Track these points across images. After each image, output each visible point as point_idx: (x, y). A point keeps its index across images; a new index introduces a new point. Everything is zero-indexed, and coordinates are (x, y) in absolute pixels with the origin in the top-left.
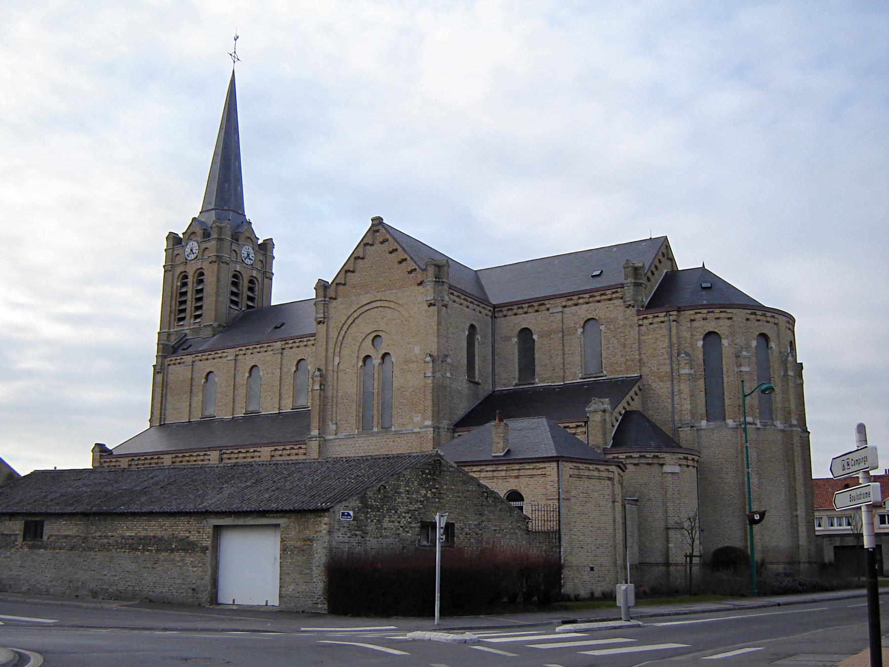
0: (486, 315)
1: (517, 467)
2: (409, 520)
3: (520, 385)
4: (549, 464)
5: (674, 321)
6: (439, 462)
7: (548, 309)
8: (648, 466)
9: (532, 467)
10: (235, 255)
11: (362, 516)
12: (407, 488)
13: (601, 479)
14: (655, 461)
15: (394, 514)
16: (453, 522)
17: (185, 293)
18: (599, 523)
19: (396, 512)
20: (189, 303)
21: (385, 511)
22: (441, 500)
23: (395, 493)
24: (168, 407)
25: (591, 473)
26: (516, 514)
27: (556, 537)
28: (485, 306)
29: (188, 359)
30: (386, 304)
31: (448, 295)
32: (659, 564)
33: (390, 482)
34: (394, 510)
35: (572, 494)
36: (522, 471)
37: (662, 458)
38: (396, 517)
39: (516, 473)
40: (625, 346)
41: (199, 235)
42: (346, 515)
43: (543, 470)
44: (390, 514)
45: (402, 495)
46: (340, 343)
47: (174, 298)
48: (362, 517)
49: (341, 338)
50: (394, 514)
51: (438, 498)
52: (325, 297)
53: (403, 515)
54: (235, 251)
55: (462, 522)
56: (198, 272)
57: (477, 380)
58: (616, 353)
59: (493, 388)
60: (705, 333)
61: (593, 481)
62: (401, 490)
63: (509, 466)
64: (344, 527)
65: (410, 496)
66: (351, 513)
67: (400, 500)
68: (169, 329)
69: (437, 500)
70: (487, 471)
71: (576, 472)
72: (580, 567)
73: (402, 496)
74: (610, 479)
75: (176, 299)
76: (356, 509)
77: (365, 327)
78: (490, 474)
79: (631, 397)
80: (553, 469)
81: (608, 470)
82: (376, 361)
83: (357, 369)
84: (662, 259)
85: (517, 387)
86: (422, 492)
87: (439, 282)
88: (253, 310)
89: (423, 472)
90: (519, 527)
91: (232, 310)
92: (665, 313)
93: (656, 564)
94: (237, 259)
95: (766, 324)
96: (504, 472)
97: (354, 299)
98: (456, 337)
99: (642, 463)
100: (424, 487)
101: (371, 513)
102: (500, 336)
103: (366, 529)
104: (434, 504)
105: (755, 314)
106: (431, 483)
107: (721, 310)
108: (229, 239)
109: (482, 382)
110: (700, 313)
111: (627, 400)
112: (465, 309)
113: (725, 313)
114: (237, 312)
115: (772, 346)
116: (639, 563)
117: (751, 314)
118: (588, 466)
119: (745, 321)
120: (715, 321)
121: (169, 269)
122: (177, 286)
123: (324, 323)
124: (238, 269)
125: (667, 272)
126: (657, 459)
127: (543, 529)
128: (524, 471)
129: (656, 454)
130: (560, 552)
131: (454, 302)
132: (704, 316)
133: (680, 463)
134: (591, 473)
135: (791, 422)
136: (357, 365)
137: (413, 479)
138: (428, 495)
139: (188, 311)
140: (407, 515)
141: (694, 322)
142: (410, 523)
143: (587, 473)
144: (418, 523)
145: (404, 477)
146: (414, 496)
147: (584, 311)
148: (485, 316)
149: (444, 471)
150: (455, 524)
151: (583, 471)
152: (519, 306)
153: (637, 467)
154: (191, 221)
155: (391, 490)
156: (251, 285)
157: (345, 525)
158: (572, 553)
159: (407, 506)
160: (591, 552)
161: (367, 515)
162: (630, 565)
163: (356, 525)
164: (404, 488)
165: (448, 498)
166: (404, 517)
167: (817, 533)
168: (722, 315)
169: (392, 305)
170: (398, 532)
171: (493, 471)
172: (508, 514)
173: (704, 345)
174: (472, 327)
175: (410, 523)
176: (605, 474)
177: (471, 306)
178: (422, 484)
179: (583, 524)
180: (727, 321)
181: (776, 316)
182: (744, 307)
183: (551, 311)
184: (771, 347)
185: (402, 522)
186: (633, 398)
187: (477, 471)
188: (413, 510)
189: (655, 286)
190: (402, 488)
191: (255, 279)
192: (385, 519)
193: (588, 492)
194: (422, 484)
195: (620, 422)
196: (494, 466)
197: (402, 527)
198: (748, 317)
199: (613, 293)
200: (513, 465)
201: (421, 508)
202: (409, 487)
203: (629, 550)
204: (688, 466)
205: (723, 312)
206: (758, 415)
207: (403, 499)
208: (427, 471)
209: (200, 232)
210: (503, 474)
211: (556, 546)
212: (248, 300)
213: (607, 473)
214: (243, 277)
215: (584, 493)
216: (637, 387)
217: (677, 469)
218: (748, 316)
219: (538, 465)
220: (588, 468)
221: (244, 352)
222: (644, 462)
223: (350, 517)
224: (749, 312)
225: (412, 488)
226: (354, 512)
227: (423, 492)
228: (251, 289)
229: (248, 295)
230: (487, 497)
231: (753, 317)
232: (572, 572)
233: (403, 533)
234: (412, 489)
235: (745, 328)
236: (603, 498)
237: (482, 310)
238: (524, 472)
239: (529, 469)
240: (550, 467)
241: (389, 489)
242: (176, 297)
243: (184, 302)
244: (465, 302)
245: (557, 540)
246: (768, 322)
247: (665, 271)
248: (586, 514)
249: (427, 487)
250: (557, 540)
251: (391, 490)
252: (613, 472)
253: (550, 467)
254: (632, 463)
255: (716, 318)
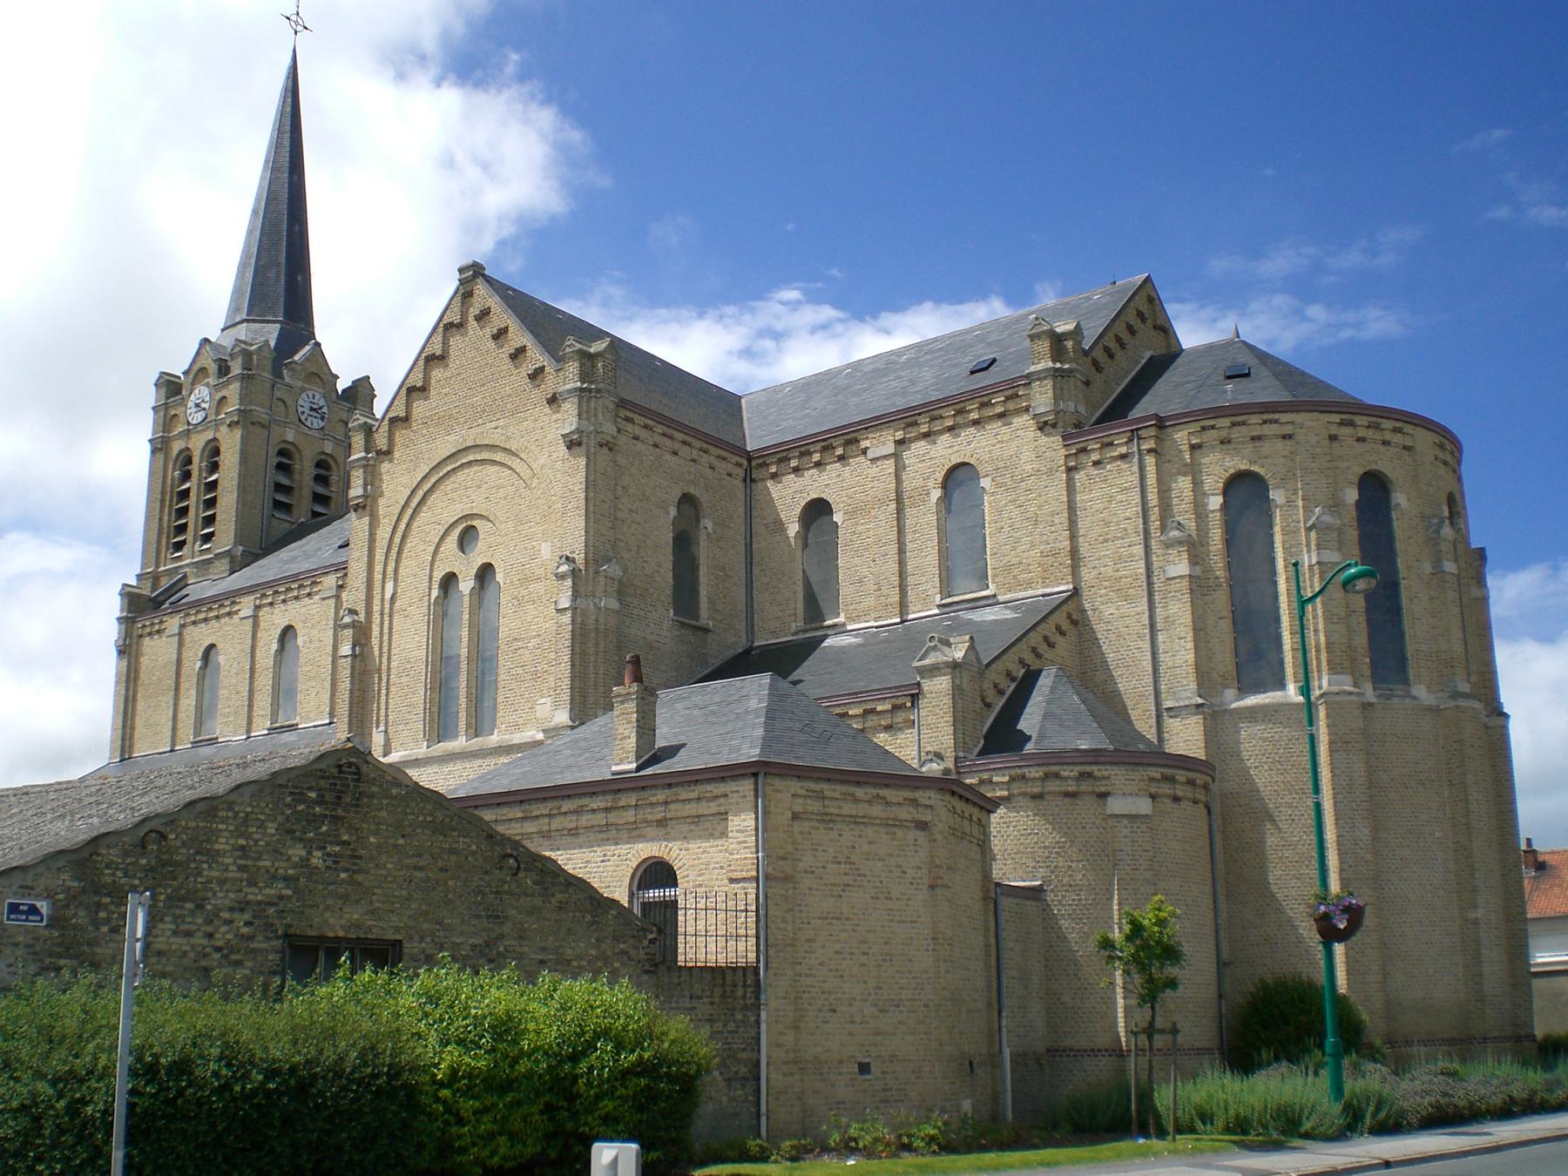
0: (729, 475)
1: (661, 796)
2: (245, 930)
3: (806, 631)
4: (733, 783)
5: (1149, 451)
6: (353, 769)
7: (864, 452)
8: (1067, 800)
9: (694, 795)
10: (282, 408)
11: (81, 917)
12: (242, 842)
13: (895, 825)
14: (1085, 786)
15: (192, 913)
16: (398, 937)
17: (185, 494)
18: (886, 943)
19: (200, 907)
20: (192, 512)
21: (161, 904)
22: (360, 878)
23: (197, 853)
24: (139, 722)
25: (861, 810)
26: (615, 917)
27: (745, 981)
28: (725, 454)
29: (173, 623)
30: (485, 455)
31: (615, 422)
32: (1099, 1050)
33: (184, 823)
34: (193, 901)
35: (800, 864)
36: (672, 806)
37: (1105, 778)
38: (200, 921)
39: (658, 813)
40: (1036, 523)
41: (210, 372)
42: (22, 912)
43: (722, 800)
44: (178, 912)
45: (220, 860)
46: (397, 550)
47: (167, 504)
48: (81, 917)
49: (397, 540)
50: (192, 913)
51: (346, 870)
52: (367, 451)
53: (226, 915)
54: (283, 402)
55: (429, 939)
56: (209, 447)
57: (703, 622)
58: (1018, 540)
59: (748, 641)
60: (1227, 475)
61: (870, 831)
62: (217, 847)
63: (643, 794)
64: (16, 945)
65: (250, 863)
66: (43, 906)
67: (216, 874)
68: (157, 566)
69: (343, 875)
70: (594, 811)
71: (814, 806)
72: (826, 1062)
73: (223, 864)
74: (922, 826)
75: (170, 506)
76: (61, 896)
77: (445, 509)
78: (600, 819)
79: (1046, 639)
80: (744, 796)
81: (915, 803)
82: (466, 585)
83: (429, 606)
84: (1137, 324)
85: (801, 636)
86: (290, 852)
87: (590, 391)
88: (320, 519)
89: (299, 797)
90: (624, 952)
91: (275, 522)
92: (1129, 434)
93: (1092, 1050)
94: (286, 417)
95: (1383, 449)
96: (632, 812)
97: (423, 447)
98: (640, 520)
99: (1050, 793)
100: (301, 840)
101: (112, 908)
102: (765, 522)
103: (94, 954)
104: (330, 888)
105: (1351, 424)
106: (324, 828)
107: (1265, 417)
108: (267, 375)
109: (714, 626)
110: (1213, 427)
111: (1033, 644)
112: (668, 457)
113: (1276, 425)
114: (287, 525)
115: (1399, 501)
116: (1048, 1050)
117: (1342, 424)
118: (852, 789)
119: (1327, 442)
120: (1251, 445)
121: (159, 446)
122: (173, 479)
123: (364, 507)
124: (328, 451)
125: (1151, 358)
126: (1091, 781)
127: (702, 957)
128: (679, 806)
129: (1088, 769)
130: (758, 1022)
131: (636, 438)
132: (1224, 433)
133: (1153, 790)
134: (861, 810)
135: (1456, 686)
136: (429, 595)
137: (262, 817)
138: (314, 861)
139: (191, 527)
140: (237, 915)
141: (1199, 451)
142: (251, 938)
143: (848, 809)
144: (277, 938)
145: (230, 809)
146: (261, 863)
147: (945, 451)
148: (726, 477)
149: (372, 796)
150: (406, 945)
151: (835, 803)
152: (803, 449)
153: (1038, 802)
154: (197, 346)
155: (184, 844)
156: (322, 472)
157: (20, 939)
158: (802, 1025)
159: (241, 890)
160: (861, 1023)
161: (97, 913)
162: (1011, 1055)
163: (59, 940)
164: (232, 841)
165: (383, 872)
166: (229, 922)
167: (1532, 970)
168: (1269, 430)
169: (498, 457)
170: (204, 963)
171: (607, 810)
172: (588, 918)
173: (1225, 506)
174: (687, 500)
175: (251, 938)
176: (904, 813)
177: (684, 451)
178: (293, 832)
179: (838, 947)
180: (1280, 444)
181: (1408, 428)
182: (1323, 409)
183: (870, 454)
184: (1398, 504)
185: (217, 936)
186: (1052, 640)
187: (571, 812)
188: (260, 903)
189: (1118, 385)
190: (223, 840)
191: (330, 461)
192: (161, 926)
193: (854, 858)
194: (293, 832)
195: (1010, 698)
196: (609, 797)
197: (218, 949)
198: (1333, 433)
199: (1008, 398)
200: (649, 792)
201: (289, 898)
202: (248, 837)
203: (1007, 1017)
204: (1176, 799)
205: (1271, 422)
206: (1367, 672)
207: (227, 870)
208: (313, 795)
209: (213, 368)
210: (629, 815)
211: (745, 1008)
212: (275, 490)
213: (911, 809)
214: (301, 455)
215: (840, 863)
216: (1065, 615)
217: (1144, 806)
218: (1334, 430)
219: (709, 788)
220: (853, 795)
221: (270, 600)
222: (1057, 789)
223: (39, 918)
224: (1336, 418)
225: (257, 841)
226: (54, 904)
227: (298, 852)
228: (322, 480)
229: (314, 493)
230: (519, 868)
231: (1346, 431)
232: (797, 1077)
233: (220, 966)
234: (256, 845)
235: (1328, 458)
236: (900, 877)
237: (643, 433)
238: (677, 811)
239: (689, 800)
240: (736, 791)
241: (178, 843)
242: (171, 500)
243: (183, 512)
244: (668, 442)
245: (750, 990)
246: (1385, 443)
247: (1148, 355)
248: (846, 919)
249: (311, 840)
250: (750, 990)
251: (184, 844)
252: (931, 807)
253: (736, 791)
254: (1024, 794)
255: (1253, 439)
